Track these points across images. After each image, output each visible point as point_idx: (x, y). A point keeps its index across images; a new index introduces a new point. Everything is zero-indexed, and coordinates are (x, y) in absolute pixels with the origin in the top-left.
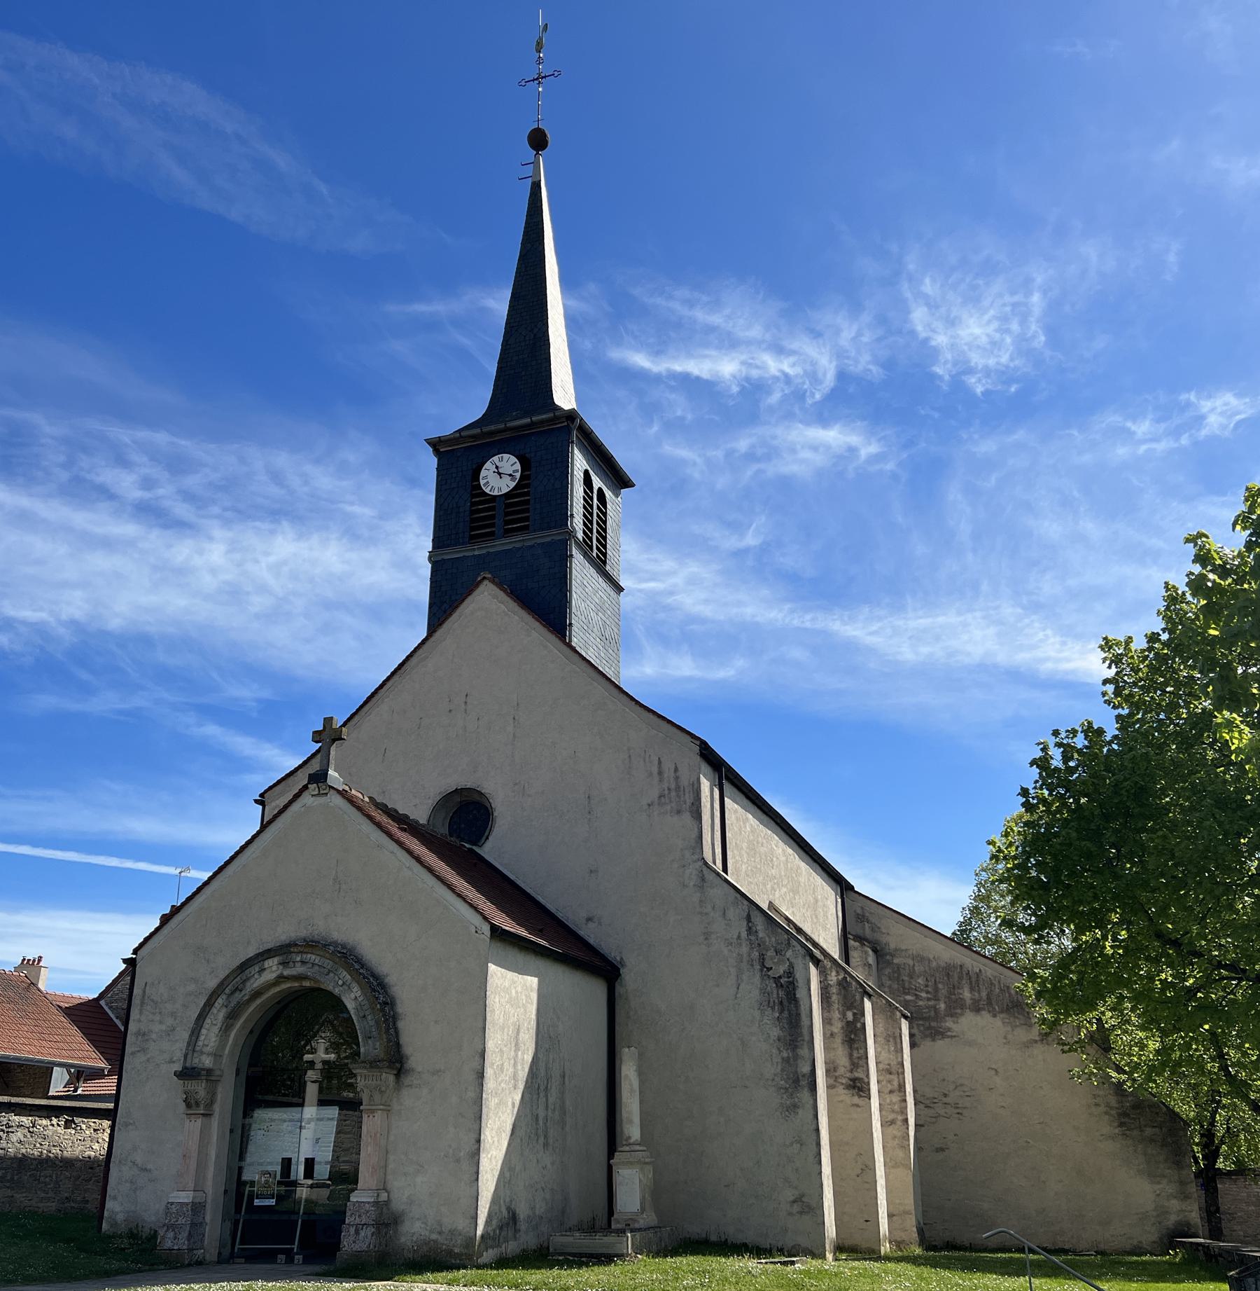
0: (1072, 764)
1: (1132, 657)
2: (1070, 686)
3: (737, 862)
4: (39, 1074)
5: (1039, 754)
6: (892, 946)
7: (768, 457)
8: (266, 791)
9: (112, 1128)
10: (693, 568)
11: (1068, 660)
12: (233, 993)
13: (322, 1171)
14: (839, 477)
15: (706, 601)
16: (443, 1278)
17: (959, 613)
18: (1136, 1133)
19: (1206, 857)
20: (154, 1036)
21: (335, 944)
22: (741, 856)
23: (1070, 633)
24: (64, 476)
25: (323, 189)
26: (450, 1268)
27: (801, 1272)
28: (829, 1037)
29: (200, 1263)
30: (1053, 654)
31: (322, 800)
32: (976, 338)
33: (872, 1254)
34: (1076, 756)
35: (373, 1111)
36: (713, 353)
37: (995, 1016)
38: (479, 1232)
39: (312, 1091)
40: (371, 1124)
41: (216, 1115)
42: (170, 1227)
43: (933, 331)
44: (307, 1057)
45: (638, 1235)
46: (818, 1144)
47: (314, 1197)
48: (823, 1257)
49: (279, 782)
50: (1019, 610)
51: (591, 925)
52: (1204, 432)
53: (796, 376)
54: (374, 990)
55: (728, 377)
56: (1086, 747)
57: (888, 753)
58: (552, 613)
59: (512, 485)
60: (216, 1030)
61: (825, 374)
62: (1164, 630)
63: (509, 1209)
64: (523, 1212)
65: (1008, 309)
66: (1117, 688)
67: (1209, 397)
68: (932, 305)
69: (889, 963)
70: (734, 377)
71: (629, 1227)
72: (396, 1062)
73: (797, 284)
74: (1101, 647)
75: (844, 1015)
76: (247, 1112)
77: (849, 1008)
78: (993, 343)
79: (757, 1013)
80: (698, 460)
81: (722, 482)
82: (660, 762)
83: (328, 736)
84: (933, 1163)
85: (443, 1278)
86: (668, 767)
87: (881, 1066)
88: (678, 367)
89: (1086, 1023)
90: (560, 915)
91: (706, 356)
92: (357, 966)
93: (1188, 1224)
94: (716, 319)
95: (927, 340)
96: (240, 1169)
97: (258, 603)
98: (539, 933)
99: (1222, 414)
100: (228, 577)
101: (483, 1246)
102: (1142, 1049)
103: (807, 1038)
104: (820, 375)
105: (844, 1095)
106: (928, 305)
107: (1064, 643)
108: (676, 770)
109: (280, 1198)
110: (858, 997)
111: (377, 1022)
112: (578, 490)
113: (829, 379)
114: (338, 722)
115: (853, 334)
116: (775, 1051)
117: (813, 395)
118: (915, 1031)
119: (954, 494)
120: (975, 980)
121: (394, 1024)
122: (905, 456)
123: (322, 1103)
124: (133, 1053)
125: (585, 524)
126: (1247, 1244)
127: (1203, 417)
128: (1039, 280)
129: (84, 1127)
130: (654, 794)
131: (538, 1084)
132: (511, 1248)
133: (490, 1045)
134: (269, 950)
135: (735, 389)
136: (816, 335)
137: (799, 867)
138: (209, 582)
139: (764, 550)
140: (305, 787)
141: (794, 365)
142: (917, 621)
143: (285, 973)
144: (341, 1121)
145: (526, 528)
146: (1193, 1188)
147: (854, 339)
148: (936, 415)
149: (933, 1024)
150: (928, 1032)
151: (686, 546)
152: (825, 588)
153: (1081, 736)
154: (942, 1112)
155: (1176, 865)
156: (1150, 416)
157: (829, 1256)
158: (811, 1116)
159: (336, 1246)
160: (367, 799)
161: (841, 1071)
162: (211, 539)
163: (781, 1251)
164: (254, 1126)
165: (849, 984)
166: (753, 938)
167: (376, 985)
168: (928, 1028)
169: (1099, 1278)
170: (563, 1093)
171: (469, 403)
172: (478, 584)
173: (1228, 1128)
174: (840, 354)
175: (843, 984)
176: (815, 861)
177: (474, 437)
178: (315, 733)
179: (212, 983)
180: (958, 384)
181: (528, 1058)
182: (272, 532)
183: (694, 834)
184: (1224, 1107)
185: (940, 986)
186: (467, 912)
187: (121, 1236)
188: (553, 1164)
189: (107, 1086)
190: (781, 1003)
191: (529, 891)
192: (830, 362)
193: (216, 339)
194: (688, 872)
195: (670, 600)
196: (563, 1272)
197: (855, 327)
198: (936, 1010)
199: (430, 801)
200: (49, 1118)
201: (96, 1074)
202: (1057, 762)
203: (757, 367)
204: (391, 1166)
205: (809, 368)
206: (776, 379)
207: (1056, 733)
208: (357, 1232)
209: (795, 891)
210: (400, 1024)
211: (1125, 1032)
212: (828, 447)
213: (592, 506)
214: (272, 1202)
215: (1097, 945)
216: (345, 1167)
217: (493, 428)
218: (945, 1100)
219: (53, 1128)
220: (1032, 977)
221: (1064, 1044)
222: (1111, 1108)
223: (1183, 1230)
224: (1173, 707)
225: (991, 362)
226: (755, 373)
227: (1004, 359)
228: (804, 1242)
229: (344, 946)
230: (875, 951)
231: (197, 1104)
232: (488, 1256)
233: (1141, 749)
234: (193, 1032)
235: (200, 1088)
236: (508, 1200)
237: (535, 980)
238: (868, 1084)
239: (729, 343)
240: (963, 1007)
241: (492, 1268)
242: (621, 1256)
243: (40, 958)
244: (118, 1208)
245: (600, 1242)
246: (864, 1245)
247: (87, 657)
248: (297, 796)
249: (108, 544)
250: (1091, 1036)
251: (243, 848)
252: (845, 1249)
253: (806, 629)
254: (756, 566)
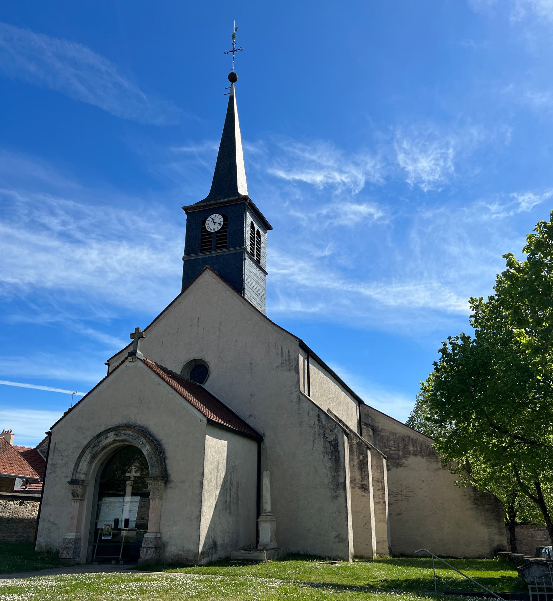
0: (456, 351)
1: (482, 306)
2: (458, 317)
3: (314, 392)
4: (11, 481)
5: (442, 347)
6: (380, 428)
7: (335, 217)
8: (110, 359)
9: (40, 505)
10: (302, 264)
11: (460, 306)
12: (94, 447)
13: (132, 525)
14: (365, 226)
15: (307, 279)
16: (184, 570)
17: (414, 285)
18: (481, 507)
19: (512, 391)
20: (59, 466)
21: (139, 426)
22: (316, 389)
23: (460, 294)
24: (27, 219)
25: (144, 96)
26: (187, 566)
27: (338, 567)
28: (352, 467)
29: (78, 564)
30: (453, 303)
31: (134, 364)
32: (424, 168)
33: (369, 559)
34: (458, 348)
35: (154, 499)
36: (312, 172)
37: (423, 458)
38: (200, 550)
39: (129, 489)
40: (154, 504)
41: (86, 500)
42: (65, 549)
43: (407, 164)
44: (127, 475)
45: (269, 552)
46: (347, 513)
47: (129, 535)
48: (348, 561)
49: (116, 355)
50: (440, 285)
51: (251, 418)
52: (520, 210)
53: (348, 182)
54: (156, 446)
55: (319, 182)
56: (462, 345)
57: (378, 345)
58: (236, 282)
59: (220, 227)
60: (86, 463)
61: (360, 181)
62: (496, 295)
63: (213, 541)
64: (219, 542)
65: (439, 155)
66: (476, 319)
67: (522, 195)
68: (406, 153)
69: (379, 435)
70: (321, 182)
71: (265, 548)
72: (165, 477)
73: (349, 142)
74: (470, 302)
75: (359, 458)
76: (100, 499)
77: (361, 455)
78: (432, 170)
79: (321, 456)
80: (305, 217)
81: (315, 228)
82: (282, 349)
83: (137, 336)
84: (396, 521)
85: (184, 570)
86: (285, 351)
87: (374, 479)
88: (297, 177)
89: (460, 462)
90: (237, 414)
91: (310, 173)
92: (148, 436)
93: (502, 546)
94: (314, 157)
95: (404, 168)
96: (96, 524)
97: (111, 276)
98: (228, 422)
99: (528, 202)
100: (99, 265)
101: (202, 557)
102: (484, 472)
103: (342, 467)
104: (358, 182)
105: (358, 491)
106: (405, 153)
107: (458, 299)
108: (289, 352)
109: (114, 536)
110: (365, 449)
111: (157, 460)
112: (248, 230)
113: (362, 184)
114: (142, 330)
115: (372, 165)
116: (329, 473)
117: (355, 191)
118: (389, 464)
119: (413, 234)
120: (415, 443)
121: (164, 461)
122: (393, 217)
123: (133, 494)
124: (50, 473)
125: (251, 245)
126: (526, 553)
127: (519, 204)
128: (453, 143)
129: (28, 505)
130: (279, 362)
131: (226, 487)
132: (214, 557)
133: (206, 470)
134: (110, 429)
135: (322, 187)
136: (356, 164)
137: (341, 394)
138: (90, 267)
139: (332, 257)
140: (127, 358)
141: (347, 178)
142: (396, 288)
143: (117, 439)
144: (141, 501)
145: (225, 246)
146: (505, 531)
147: (373, 167)
148: (407, 200)
149: (397, 461)
150: (395, 465)
151: (299, 255)
152: (358, 274)
153: (460, 340)
154: (400, 499)
155: (499, 395)
156: (497, 203)
157: (351, 560)
158: (344, 500)
159: (138, 557)
160: (154, 363)
161: (357, 481)
162: (91, 248)
163: (330, 558)
164: (103, 505)
165: (361, 444)
166: (320, 424)
167: (157, 444)
168: (394, 462)
169: (464, 569)
170: (237, 491)
171: (201, 191)
172: (204, 271)
173: (520, 505)
174: (367, 174)
175: (359, 444)
176: (348, 391)
177: (203, 206)
178: (131, 334)
179: (85, 443)
180: (417, 188)
181: (223, 476)
182: (119, 246)
183: (296, 380)
184: (518, 496)
185: (400, 445)
186: (198, 413)
187: (43, 553)
188: (233, 521)
189: (38, 487)
190: (332, 452)
191: (224, 403)
192: (363, 176)
193: (94, 159)
194: (293, 396)
195: (291, 278)
196: (236, 568)
197: (373, 162)
198: (398, 455)
199: (182, 365)
200: (13, 501)
201: (35, 481)
202: (450, 350)
203: (331, 178)
204: (162, 522)
205: (353, 179)
206: (339, 183)
207: (450, 338)
208: (147, 551)
209: (339, 404)
210: (167, 461)
211: (478, 465)
212: (361, 213)
213: (254, 238)
214: (110, 538)
215: (466, 429)
216: (142, 522)
217: (211, 202)
218: (402, 493)
219: (14, 505)
220: (437, 440)
221: (452, 470)
222: (471, 497)
223: (501, 548)
224: (499, 328)
225: (431, 178)
226: (330, 181)
227: (437, 177)
228: (340, 554)
229: (143, 427)
230: (373, 430)
231: (78, 495)
232: (204, 561)
233: (486, 346)
234: (76, 464)
235: (79, 488)
236: (213, 536)
237: (226, 442)
238: (369, 487)
239: (319, 167)
240: (409, 454)
241: (205, 566)
242: (261, 561)
243: (11, 431)
244: (42, 541)
245: (252, 555)
246: (366, 555)
247: (34, 299)
248: (123, 362)
249: (46, 250)
250: (463, 467)
251: (99, 384)
252: (358, 557)
253: (349, 291)
254: (328, 264)
